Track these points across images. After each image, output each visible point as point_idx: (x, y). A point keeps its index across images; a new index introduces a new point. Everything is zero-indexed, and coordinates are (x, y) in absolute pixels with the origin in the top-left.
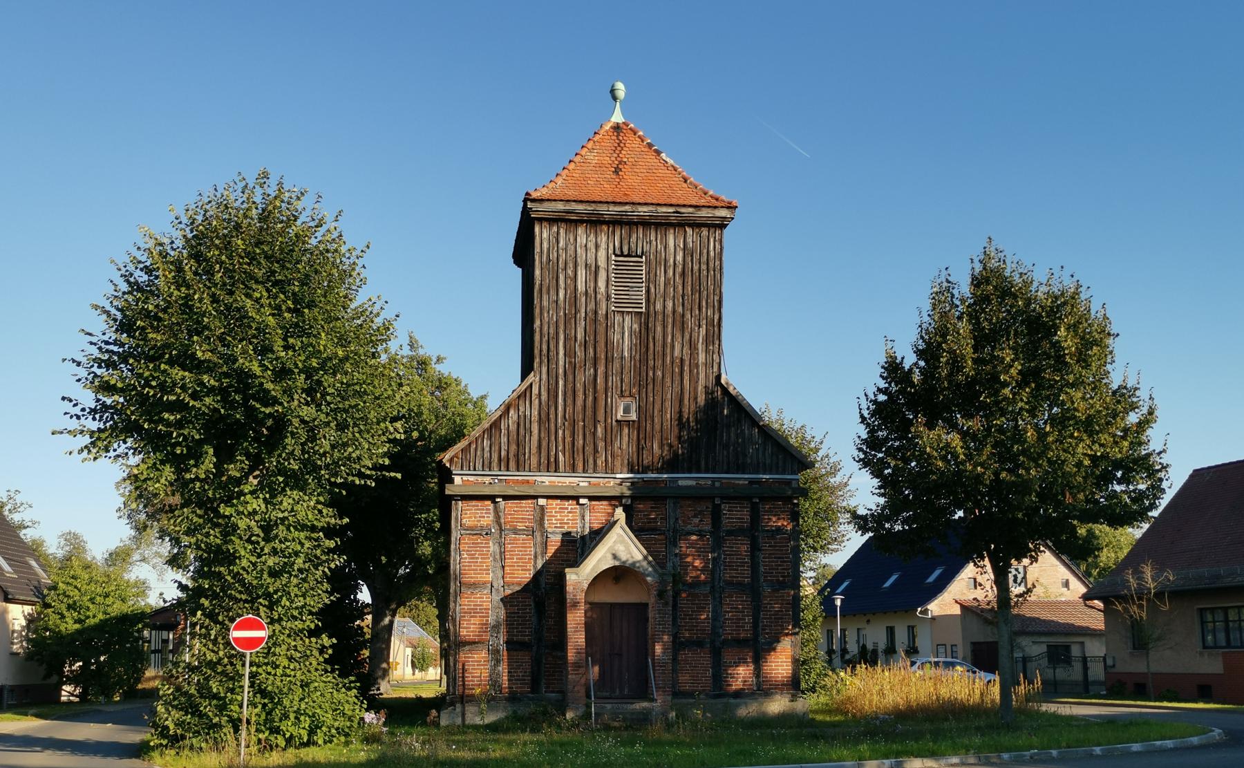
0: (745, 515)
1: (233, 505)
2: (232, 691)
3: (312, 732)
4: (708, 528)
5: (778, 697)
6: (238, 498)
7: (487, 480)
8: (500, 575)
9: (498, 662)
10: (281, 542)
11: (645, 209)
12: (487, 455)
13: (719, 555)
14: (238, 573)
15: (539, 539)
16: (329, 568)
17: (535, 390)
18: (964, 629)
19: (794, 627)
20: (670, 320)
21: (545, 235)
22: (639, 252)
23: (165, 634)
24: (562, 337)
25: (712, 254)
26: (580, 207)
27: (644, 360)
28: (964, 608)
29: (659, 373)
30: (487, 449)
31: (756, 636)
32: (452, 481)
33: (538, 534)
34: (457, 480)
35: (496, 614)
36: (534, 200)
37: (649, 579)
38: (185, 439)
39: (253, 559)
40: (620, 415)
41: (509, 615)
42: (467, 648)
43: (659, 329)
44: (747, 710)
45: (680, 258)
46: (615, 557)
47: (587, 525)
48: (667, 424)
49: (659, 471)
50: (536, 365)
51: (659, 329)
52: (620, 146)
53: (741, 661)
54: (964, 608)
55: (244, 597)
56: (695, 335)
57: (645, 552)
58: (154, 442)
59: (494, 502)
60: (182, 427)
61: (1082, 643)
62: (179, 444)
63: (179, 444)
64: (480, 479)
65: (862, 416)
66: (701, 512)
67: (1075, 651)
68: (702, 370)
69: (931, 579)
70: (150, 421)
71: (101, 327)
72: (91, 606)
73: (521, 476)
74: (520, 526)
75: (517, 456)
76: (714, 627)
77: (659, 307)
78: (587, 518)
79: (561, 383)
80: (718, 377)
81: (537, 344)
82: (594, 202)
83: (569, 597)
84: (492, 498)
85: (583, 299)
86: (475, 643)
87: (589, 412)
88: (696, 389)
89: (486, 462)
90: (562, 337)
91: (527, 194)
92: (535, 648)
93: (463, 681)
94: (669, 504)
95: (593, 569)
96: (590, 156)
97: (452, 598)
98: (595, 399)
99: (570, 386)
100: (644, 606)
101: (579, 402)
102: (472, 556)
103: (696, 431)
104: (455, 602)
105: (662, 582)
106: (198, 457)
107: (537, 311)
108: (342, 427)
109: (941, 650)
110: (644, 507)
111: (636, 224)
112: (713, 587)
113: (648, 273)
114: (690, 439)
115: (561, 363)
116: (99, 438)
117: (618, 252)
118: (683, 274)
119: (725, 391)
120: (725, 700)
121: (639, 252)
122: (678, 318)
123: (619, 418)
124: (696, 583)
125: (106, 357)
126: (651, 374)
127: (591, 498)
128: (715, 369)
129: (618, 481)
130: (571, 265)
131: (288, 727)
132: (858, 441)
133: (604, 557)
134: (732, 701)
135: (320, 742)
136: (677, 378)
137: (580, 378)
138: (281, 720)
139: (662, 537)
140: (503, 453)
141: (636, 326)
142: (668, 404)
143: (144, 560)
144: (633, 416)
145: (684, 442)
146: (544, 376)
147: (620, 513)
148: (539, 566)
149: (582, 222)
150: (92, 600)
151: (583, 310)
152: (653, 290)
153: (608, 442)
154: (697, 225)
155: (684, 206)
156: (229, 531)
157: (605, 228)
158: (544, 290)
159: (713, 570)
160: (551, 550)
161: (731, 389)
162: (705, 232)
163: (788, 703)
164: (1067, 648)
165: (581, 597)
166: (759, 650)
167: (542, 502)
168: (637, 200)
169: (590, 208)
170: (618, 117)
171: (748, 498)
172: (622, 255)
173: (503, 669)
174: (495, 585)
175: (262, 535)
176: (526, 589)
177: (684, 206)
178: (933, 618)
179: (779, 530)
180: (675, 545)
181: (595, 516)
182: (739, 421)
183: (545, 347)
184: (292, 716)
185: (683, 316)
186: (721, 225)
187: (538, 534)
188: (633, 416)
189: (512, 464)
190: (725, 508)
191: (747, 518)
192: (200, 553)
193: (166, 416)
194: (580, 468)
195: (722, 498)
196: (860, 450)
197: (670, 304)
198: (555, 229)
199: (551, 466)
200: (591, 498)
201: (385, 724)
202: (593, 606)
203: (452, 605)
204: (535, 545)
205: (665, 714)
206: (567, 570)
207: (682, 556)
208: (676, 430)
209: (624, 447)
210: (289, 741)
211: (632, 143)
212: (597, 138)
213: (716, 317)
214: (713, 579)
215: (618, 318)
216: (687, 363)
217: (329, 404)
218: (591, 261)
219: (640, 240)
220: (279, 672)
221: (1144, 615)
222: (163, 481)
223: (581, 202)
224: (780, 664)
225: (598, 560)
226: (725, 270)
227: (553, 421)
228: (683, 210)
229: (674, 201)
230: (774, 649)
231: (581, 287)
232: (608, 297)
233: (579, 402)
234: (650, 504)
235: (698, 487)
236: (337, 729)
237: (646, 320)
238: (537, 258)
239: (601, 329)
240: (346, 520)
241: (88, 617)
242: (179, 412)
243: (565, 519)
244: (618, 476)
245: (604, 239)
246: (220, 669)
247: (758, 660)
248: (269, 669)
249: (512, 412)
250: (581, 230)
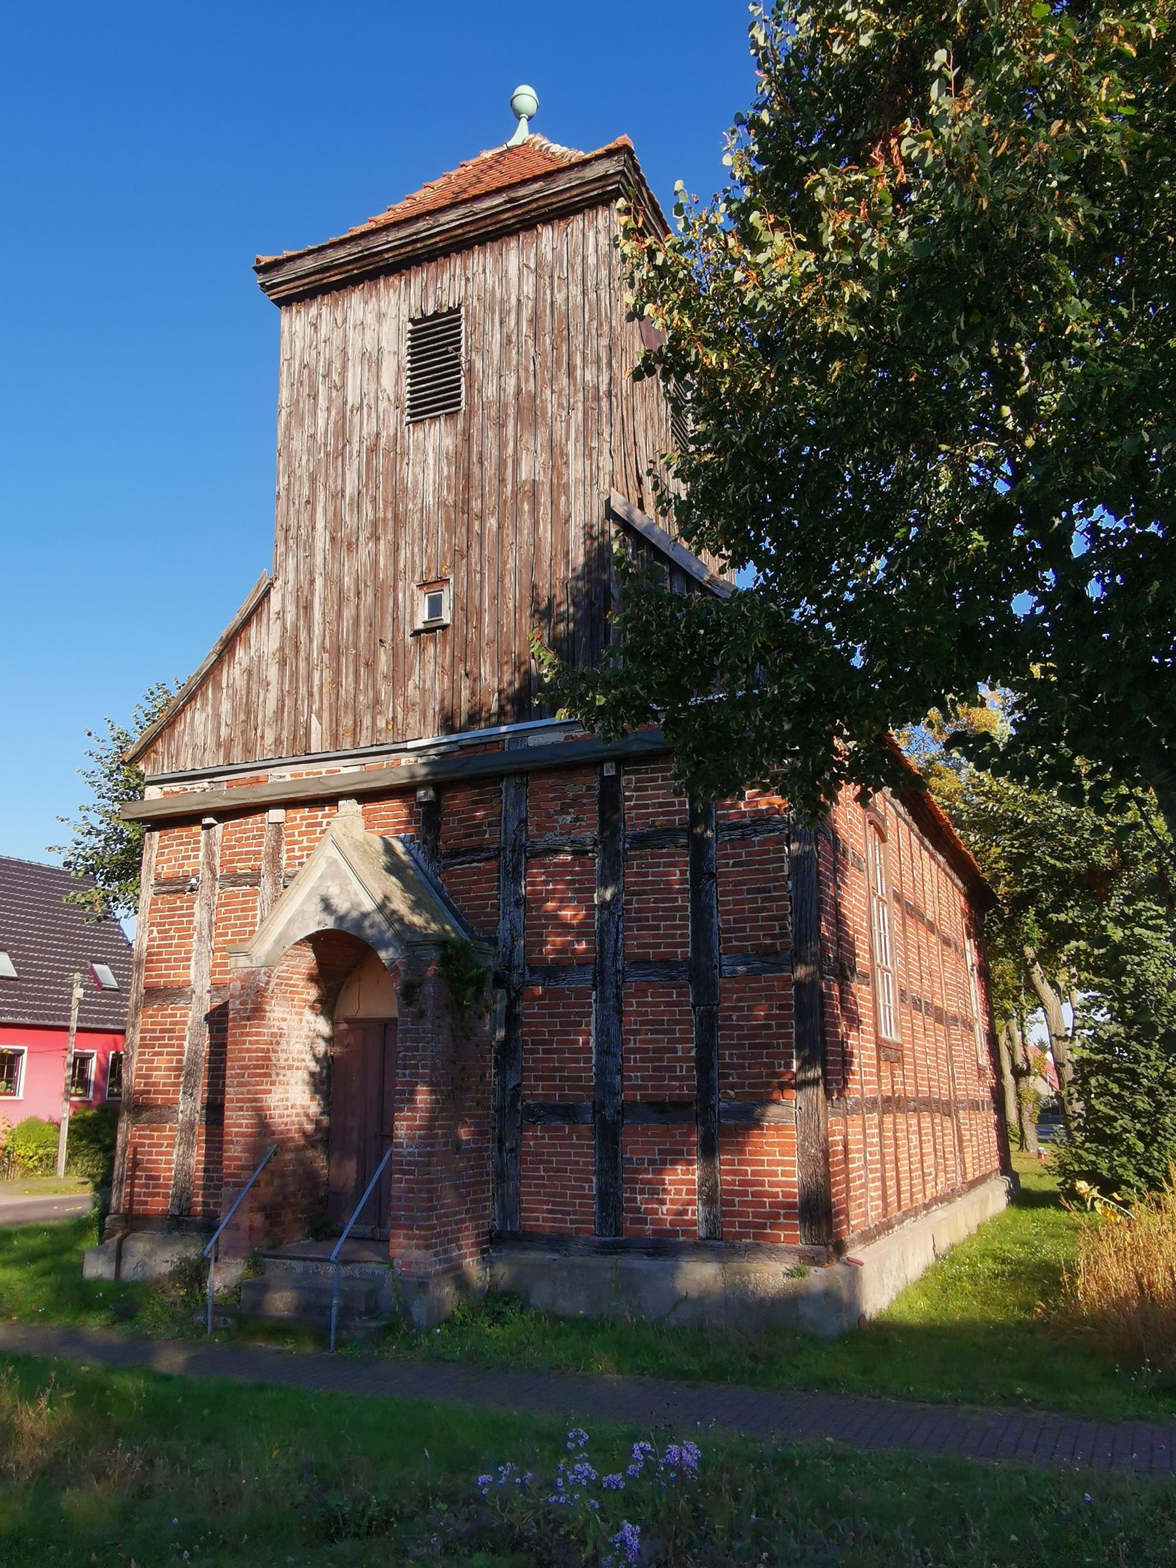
4: (590, 834)
19: (806, 1064)
25: (592, 260)
26: (340, 254)
31: (706, 1088)
45: (528, 288)
48: (507, 621)
53: (674, 1156)
76: (602, 1070)
88: (565, 537)
118: (535, 320)
133: (301, 912)
134: (643, 1263)
139: (493, 864)
153: (398, 678)
155: (524, 183)
167: (276, 815)
177: (524, 183)
198: (313, 311)
234: (474, 794)
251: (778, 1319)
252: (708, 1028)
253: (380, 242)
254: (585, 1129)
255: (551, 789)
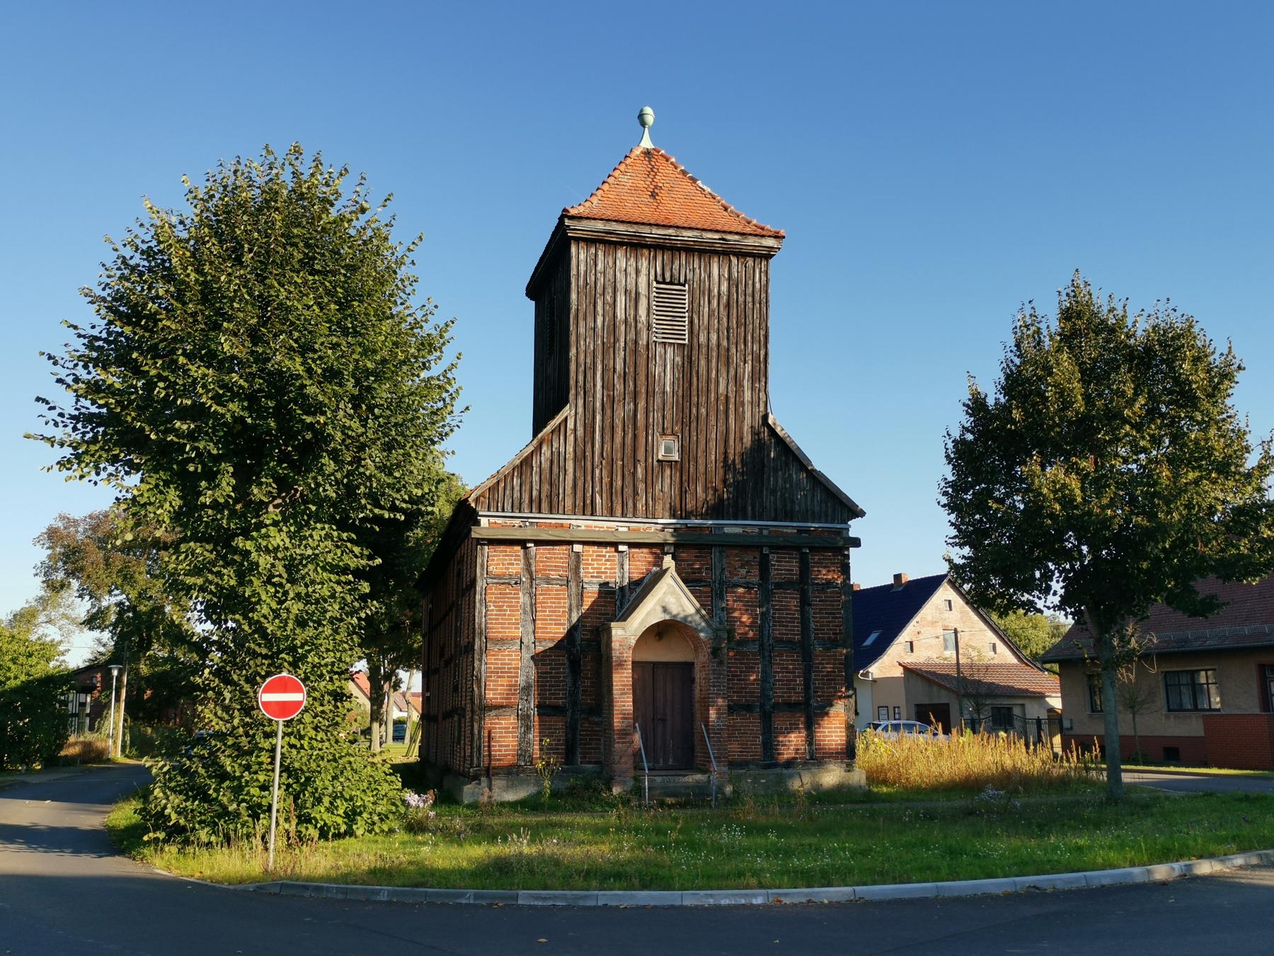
0: (794, 566)
1: (252, 539)
2: (247, 767)
3: (351, 816)
4: (756, 580)
5: (832, 767)
6: (258, 530)
7: (517, 522)
8: (531, 628)
9: (528, 728)
10: (306, 586)
11: (690, 233)
12: (517, 495)
13: (768, 610)
14: (258, 621)
15: (574, 589)
16: (1127, 520)
17: (570, 425)
18: (907, 691)
19: (847, 689)
20: (714, 354)
21: (582, 257)
22: (682, 280)
23: (82, 696)
24: (599, 367)
25: (758, 285)
26: (621, 228)
27: (687, 395)
28: (907, 669)
29: (703, 411)
30: (517, 488)
31: (808, 698)
32: (478, 523)
33: (573, 584)
34: (484, 522)
35: (525, 672)
36: (572, 218)
37: (702, 635)
38: (199, 454)
39: (274, 606)
40: (661, 454)
41: (541, 677)
42: (493, 713)
43: (703, 363)
44: (801, 783)
45: (724, 288)
46: (665, 610)
47: (627, 575)
49: (703, 517)
50: (571, 397)
51: (703, 363)
52: (653, 171)
54: (907, 669)
55: (264, 651)
56: (740, 371)
57: (698, 605)
58: (161, 458)
59: (525, 548)
60: (196, 440)
61: (1023, 705)
62: (191, 460)
63: (191, 460)
64: (508, 521)
65: (947, 456)
66: (748, 563)
67: (1017, 711)
68: (748, 408)
69: (868, 642)
70: (155, 428)
71: (93, 320)
72: (13, 667)
73: (555, 519)
74: (554, 575)
75: (550, 497)
76: (763, 690)
77: (703, 339)
78: (626, 567)
79: (598, 417)
80: (765, 417)
81: (573, 374)
82: (636, 223)
83: (615, 654)
84: (522, 543)
85: (623, 327)
86: (502, 707)
87: (629, 450)
89: (516, 503)
90: (599, 367)
91: (565, 210)
92: (569, 714)
93: (489, 751)
94: (715, 553)
95: (641, 624)
96: (624, 179)
97: (476, 656)
98: (635, 436)
99: (608, 422)
100: (689, 666)
101: (618, 439)
102: (500, 608)
103: (742, 474)
104: (480, 660)
105: (716, 638)
106: (212, 476)
107: (573, 338)
108: (388, 447)
109: (883, 711)
110: (693, 551)
111: (679, 250)
112: (761, 645)
113: (691, 303)
114: (737, 484)
115: (599, 396)
116: (86, 452)
117: (660, 279)
118: (728, 305)
119: (772, 431)
120: (778, 770)
121: (682, 280)
122: (723, 352)
123: (660, 457)
124: (744, 641)
125: (95, 354)
126: (694, 411)
127: (632, 545)
128: (762, 409)
129: (660, 527)
130: (610, 290)
131: (320, 813)
132: (943, 484)
133: (653, 609)
134: (785, 771)
135: (359, 832)
136: (722, 416)
137: (619, 413)
138: (313, 805)
139: (708, 589)
140: (535, 493)
141: (678, 359)
142: (712, 444)
143: (49, 622)
144: (676, 457)
145: (730, 485)
146: (580, 410)
147: (668, 561)
148: (574, 620)
149: (621, 244)
150: (14, 660)
151: (622, 340)
152: (696, 321)
153: (649, 482)
154: (742, 254)
155: (731, 233)
156: (246, 571)
157: (646, 252)
158: (581, 316)
159: (761, 626)
160: (588, 602)
161: (778, 430)
162: (750, 262)
163: (843, 773)
164: (1010, 709)
165: (628, 656)
166: (812, 714)
167: (577, 548)
168: (680, 224)
169: (632, 229)
170: (647, 143)
171: (798, 548)
172: (664, 282)
173: (534, 736)
174: (525, 641)
175: (285, 576)
176: (560, 645)
177: (731, 233)
178: (875, 681)
179: (829, 583)
180: (722, 598)
181: (638, 564)
182: (787, 464)
183: (581, 378)
184: (326, 800)
185: (728, 350)
186: (767, 255)
187: (573, 584)
188: (676, 457)
189: (545, 505)
190: (773, 558)
191: (796, 570)
192: (209, 597)
193: (178, 424)
194: (619, 512)
195: (771, 547)
196: (945, 494)
197: (714, 337)
198: (593, 250)
199: (588, 509)
200: (632, 545)
201: (434, 806)
202: (636, 665)
203: (476, 663)
204: (570, 596)
205: (720, 789)
206: (613, 624)
207: (729, 610)
208: (721, 472)
209: (666, 489)
210: (323, 834)
211: (665, 171)
212: (628, 161)
213: (762, 352)
214: (761, 637)
215: (659, 349)
216: (732, 400)
217: (376, 418)
218: (631, 286)
219: (683, 266)
220: (305, 743)
221: (1132, 677)
222: (167, 506)
223: (623, 222)
224: (832, 732)
225: (647, 613)
226: (770, 303)
227: (589, 458)
228: (729, 237)
229: (719, 228)
230: (827, 714)
231: (620, 314)
232: (649, 327)
233: (618, 439)
234: (694, 552)
235: (745, 535)
236: (379, 814)
237: (689, 353)
238: (573, 280)
239: (642, 361)
240: (379, 561)
241: (9, 679)
242: (193, 421)
243: (603, 569)
244: (660, 521)
245: (645, 264)
246: (230, 741)
247: (810, 727)
248: (293, 741)
249: (544, 448)
250: (620, 254)
251: (840, 794)
254: (756, 715)
255: (736, 555)
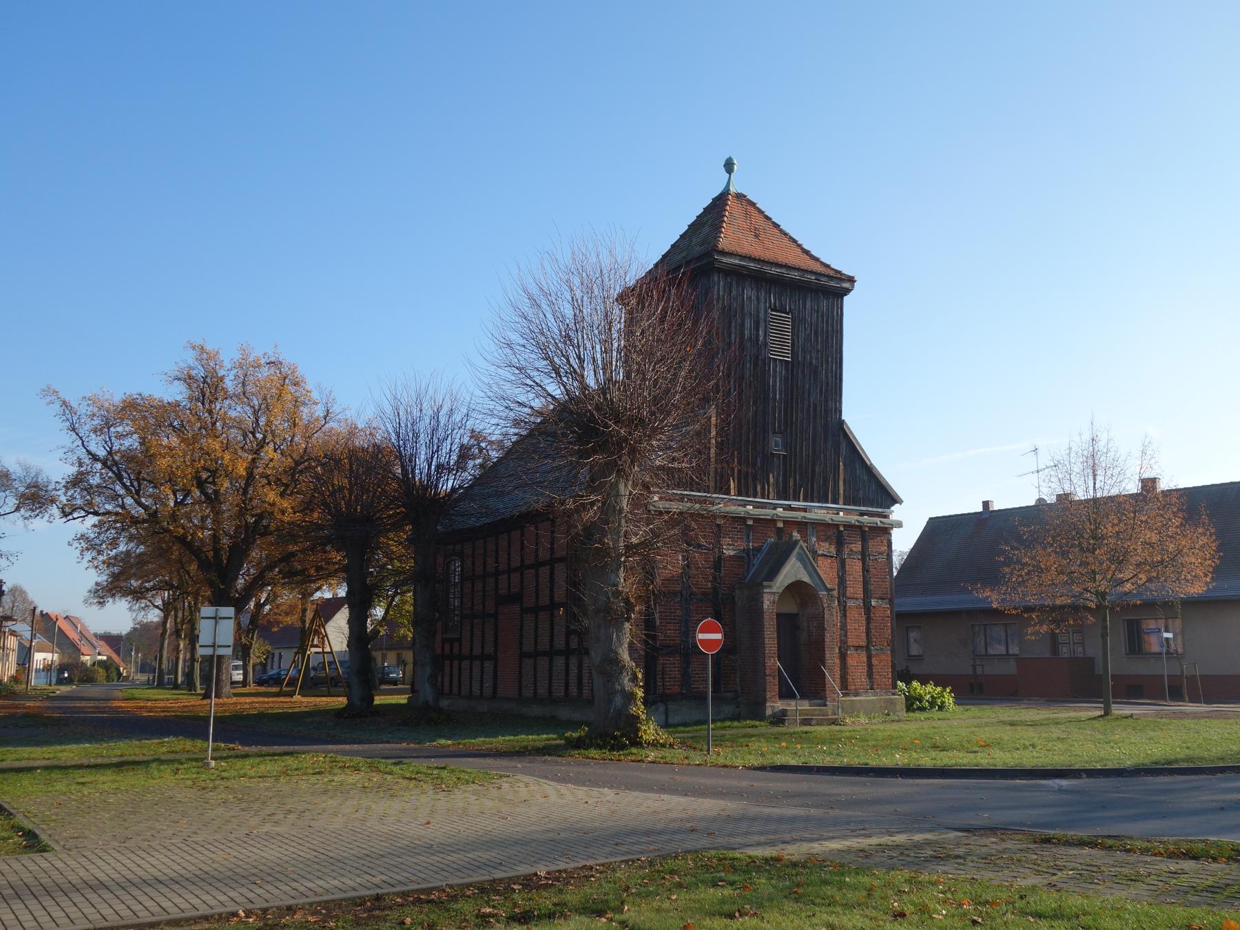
252: (868, 620)
253: (767, 269)
